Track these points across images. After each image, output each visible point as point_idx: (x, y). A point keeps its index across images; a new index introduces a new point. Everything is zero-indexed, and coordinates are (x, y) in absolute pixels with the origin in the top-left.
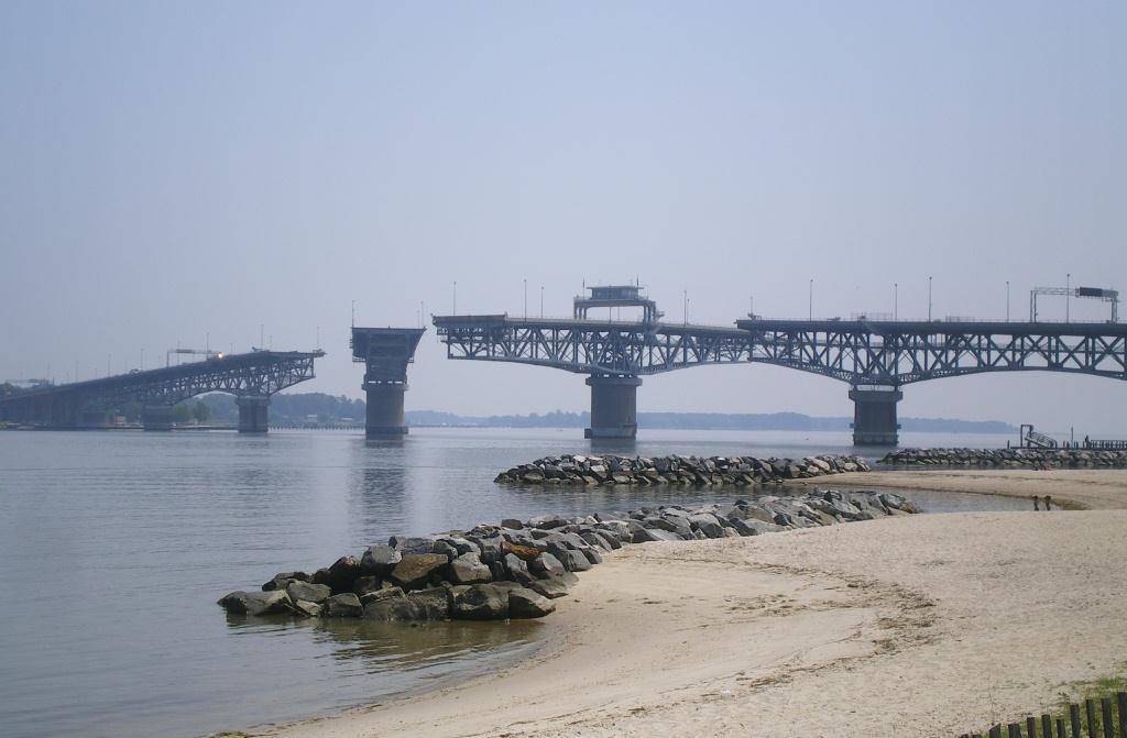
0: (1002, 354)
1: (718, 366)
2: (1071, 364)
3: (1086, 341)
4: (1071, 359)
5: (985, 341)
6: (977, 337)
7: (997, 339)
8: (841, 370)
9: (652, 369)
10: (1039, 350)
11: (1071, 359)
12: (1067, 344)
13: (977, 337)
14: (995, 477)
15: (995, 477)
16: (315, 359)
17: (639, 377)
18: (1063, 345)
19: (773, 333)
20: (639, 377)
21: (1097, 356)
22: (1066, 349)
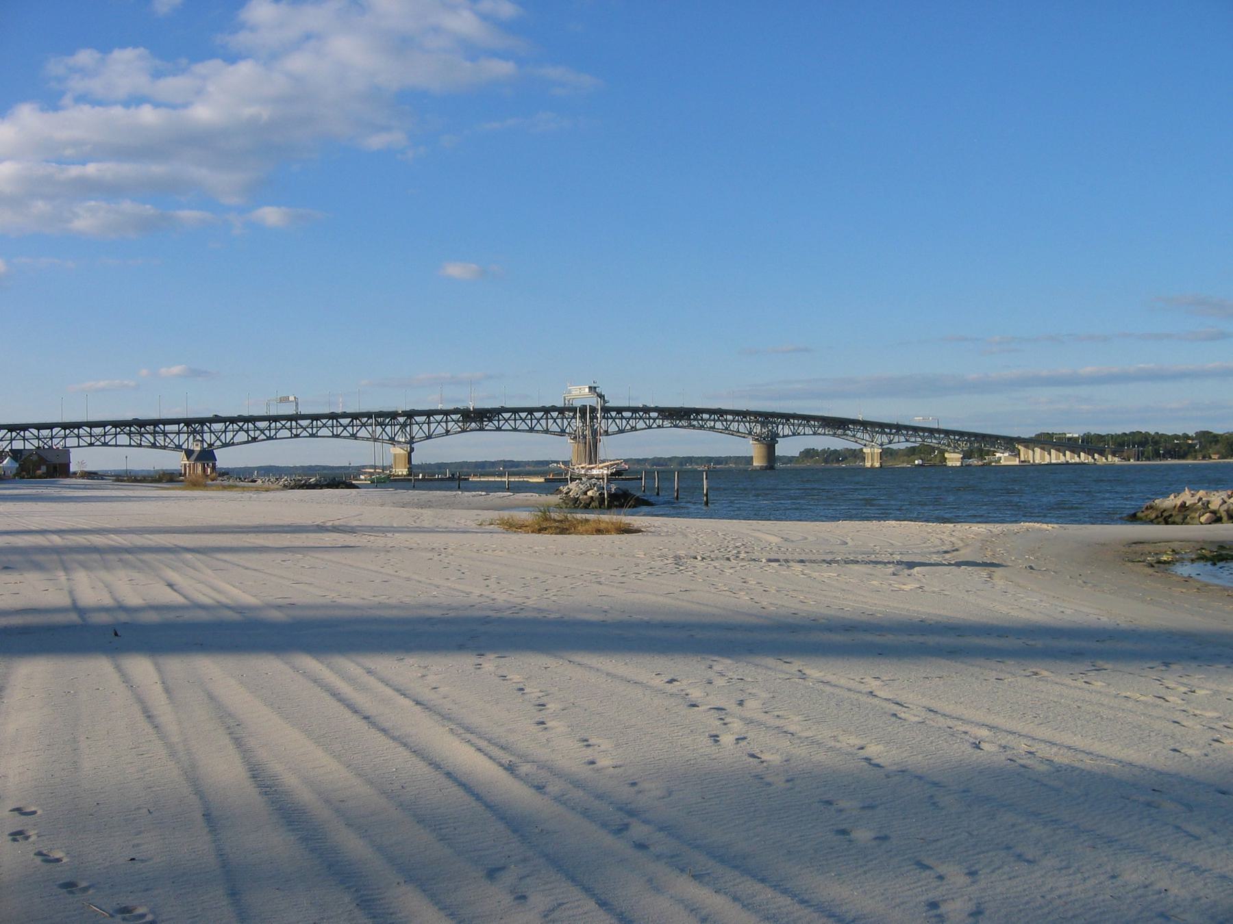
0: (241, 428)
1: (448, 437)
2: (507, 426)
3: (352, 421)
4: (345, 431)
5: (294, 423)
6: (289, 422)
7: (625, 414)
8: (738, 432)
9: (606, 433)
10: (243, 430)
11: (345, 431)
12: (302, 424)
13: (246, 424)
14: (337, 480)
15: (337, 480)
16: (246, 440)
17: (777, 439)
18: (340, 423)
19: (128, 428)
20: (777, 439)
21: (351, 424)
22: (302, 427)
